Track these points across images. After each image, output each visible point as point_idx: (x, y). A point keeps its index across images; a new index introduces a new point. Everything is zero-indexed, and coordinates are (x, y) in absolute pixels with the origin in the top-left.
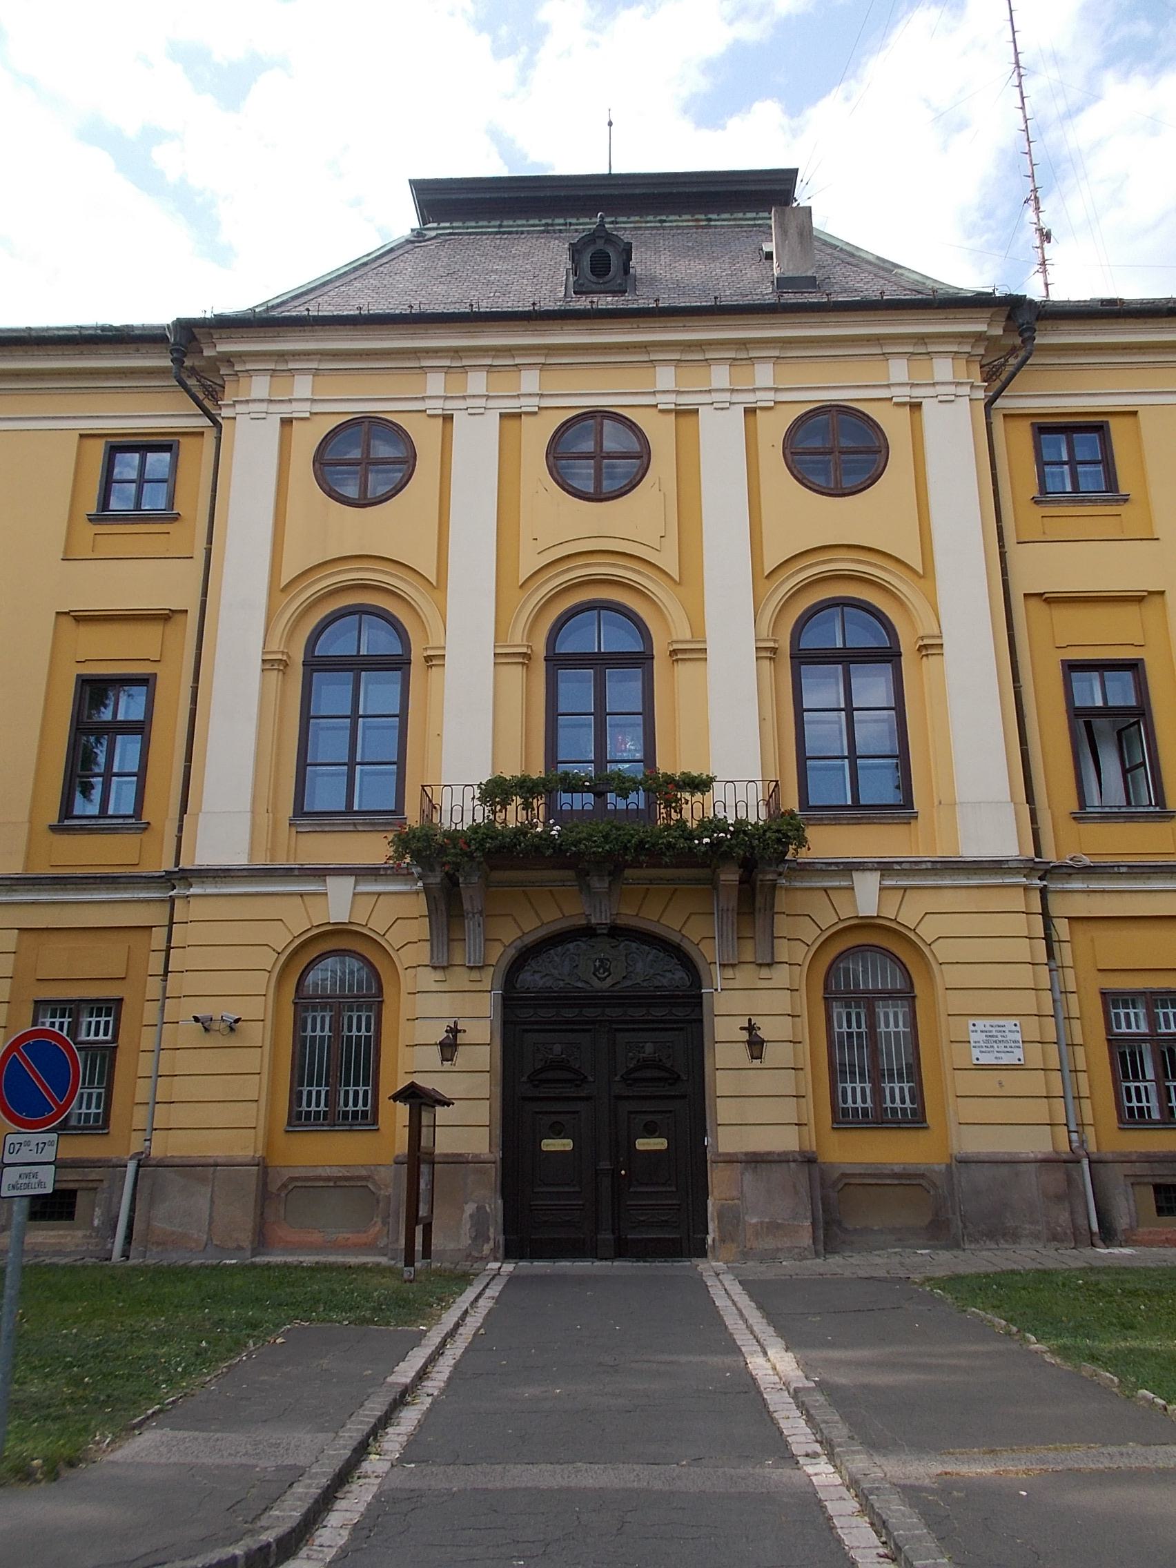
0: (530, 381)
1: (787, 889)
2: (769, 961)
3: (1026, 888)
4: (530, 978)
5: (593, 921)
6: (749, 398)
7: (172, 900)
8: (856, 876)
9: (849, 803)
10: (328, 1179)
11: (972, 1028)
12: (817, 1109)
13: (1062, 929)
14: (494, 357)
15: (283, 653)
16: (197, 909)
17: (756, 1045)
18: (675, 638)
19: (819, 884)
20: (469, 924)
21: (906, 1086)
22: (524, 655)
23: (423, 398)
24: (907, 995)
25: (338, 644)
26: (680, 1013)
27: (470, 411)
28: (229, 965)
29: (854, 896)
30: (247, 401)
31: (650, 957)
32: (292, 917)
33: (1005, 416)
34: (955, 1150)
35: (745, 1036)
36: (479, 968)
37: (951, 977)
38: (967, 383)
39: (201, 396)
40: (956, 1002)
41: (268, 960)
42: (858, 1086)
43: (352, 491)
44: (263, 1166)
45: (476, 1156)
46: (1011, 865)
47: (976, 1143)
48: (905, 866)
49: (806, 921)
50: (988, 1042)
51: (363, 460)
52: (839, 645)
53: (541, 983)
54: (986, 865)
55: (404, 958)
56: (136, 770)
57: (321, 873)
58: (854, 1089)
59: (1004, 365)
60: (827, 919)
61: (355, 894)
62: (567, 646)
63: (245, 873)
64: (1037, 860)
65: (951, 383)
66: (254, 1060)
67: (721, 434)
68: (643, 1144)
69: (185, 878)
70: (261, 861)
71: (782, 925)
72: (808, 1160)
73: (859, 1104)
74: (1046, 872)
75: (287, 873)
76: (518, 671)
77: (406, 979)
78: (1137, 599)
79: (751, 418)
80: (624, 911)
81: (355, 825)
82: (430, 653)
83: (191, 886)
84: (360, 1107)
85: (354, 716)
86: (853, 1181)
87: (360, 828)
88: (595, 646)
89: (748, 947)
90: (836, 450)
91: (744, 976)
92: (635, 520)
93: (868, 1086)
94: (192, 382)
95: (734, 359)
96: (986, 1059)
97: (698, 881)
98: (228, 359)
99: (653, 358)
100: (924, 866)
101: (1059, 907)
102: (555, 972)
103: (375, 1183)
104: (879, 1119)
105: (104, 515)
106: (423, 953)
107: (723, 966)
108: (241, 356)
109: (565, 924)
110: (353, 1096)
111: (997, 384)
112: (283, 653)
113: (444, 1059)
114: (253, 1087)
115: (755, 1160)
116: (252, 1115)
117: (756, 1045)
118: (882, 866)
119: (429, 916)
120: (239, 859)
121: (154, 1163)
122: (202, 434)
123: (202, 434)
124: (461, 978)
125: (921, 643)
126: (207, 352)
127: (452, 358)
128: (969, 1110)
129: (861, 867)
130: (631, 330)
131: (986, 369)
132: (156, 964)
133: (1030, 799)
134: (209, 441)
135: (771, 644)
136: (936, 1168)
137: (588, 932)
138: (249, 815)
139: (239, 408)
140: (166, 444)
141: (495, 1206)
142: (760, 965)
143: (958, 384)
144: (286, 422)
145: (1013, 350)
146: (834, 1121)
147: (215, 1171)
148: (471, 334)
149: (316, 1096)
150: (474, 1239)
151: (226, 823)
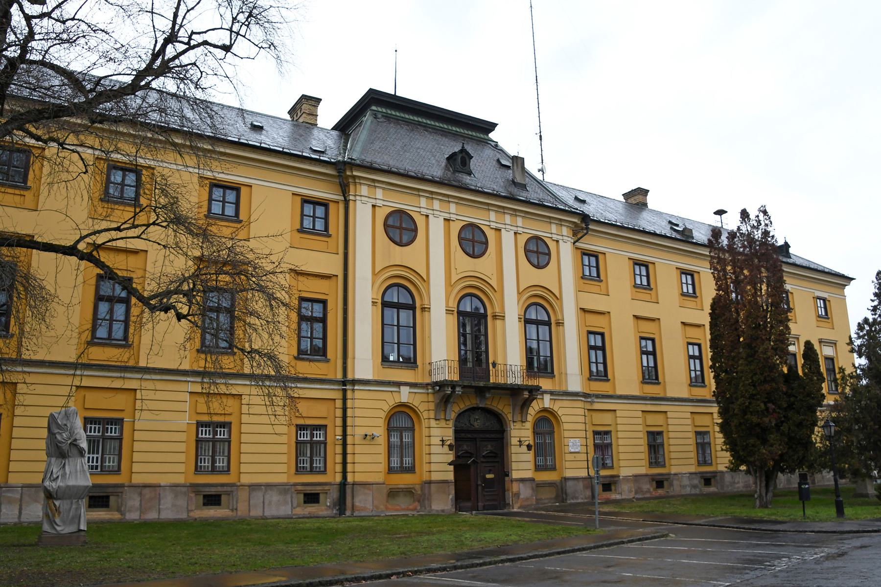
6: (374, 201)
8: (402, 387)
24: (412, 429)
26: (463, 435)
28: (369, 414)
32: (389, 399)
37: (566, 426)
47: (569, 474)
49: (535, 407)
51: (400, 228)
55: (425, 415)
57: (398, 384)
77: (425, 423)
78: (652, 320)
91: (518, 425)
92: (484, 266)
96: (572, 450)
98: (354, 177)
105: (302, 230)
106: (432, 415)
108: (360, 177)
115: (522, 480)
120: (370, 377)
124: (443, 423)
130: (518, 205)
132: (339, 413)
139: (358, 198)
140: (325, 204)
145: (582, 229)
148: (439, 188)
149: (319, 437)
151: (365, 363)
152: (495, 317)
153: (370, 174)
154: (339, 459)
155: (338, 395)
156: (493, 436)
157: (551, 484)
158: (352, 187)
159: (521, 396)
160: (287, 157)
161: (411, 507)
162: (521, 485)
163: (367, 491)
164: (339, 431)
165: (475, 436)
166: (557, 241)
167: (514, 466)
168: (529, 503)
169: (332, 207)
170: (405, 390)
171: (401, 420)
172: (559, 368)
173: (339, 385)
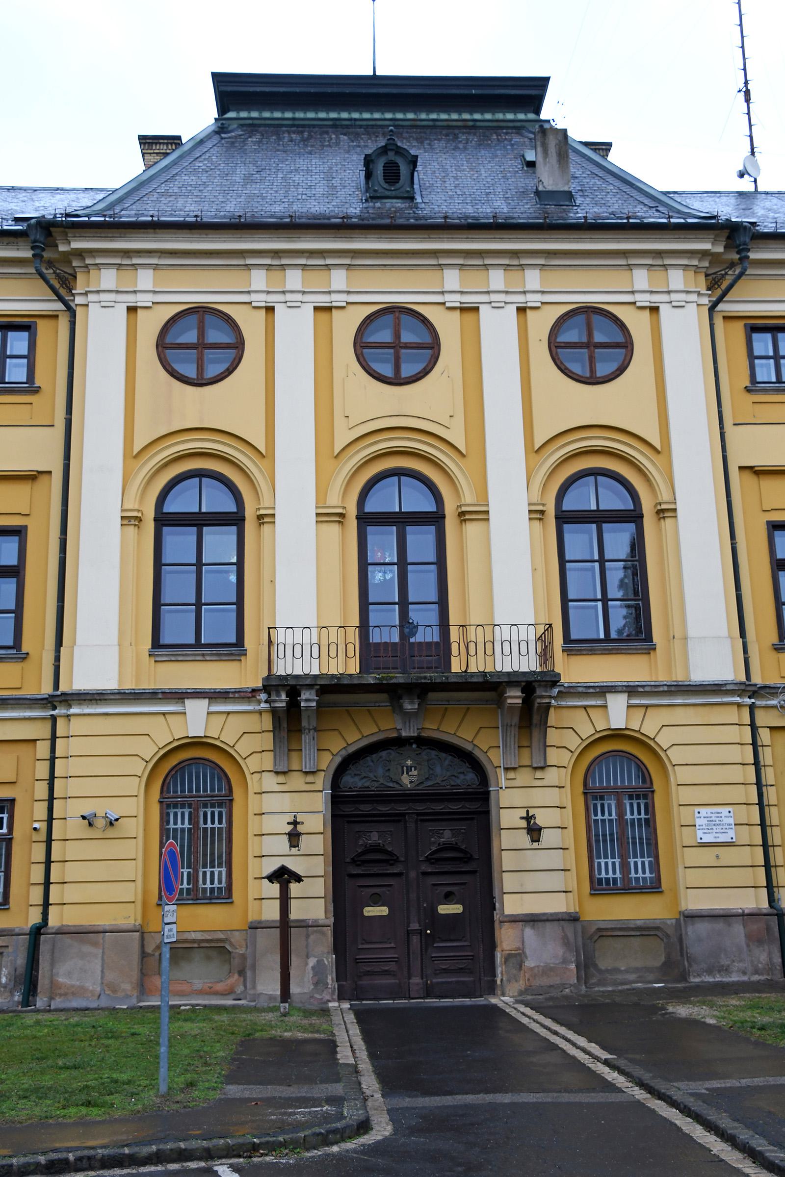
0: (339, 279)
1: (556, 707)
2: (542, 765)
3: (739, 705)
4: (352, 781)
5: (404, 734)
6: (520, 299)
7: (54, 719)
8: (609, 696)
9: (602, 636)
10: (194, 941)
11: (697, 815)
12: (576, 879)
13: (765, 736)
14: (308, 258)
15: (138, 511)
16: (77, 726)
17: (534, 831)
18: (463, 502)
19: (580, 704)
20: (306, 738)
21: (646, 861)
22: (341, 514)
23: (249, 292)
25: (182, 502)
27: (494, 305)
28: (107, 773)
29: (607, 713)
30: (98, 292)
31: (447, 762)
32: (161, 730)
33: (725, 318)
34: (683, 907)
35: (524, 824)
36: (313, 773)
37: (682, 775)
38: (695, 292)
39: (57, 286)
40: (685, 795)
41: (139, 768)
42: (610, 861)
43: (190, 371)
44: (142, 932)
45: (316, 920)
46: (729, 687)
47: (695, 902)
48: (647, 689)
49: (571, 731)
50: (709, 825)
51: (200, 346)
52: (397, 510)
53: (360, 784)
54: (709, 688)
55: (251, 765)
56: (13, 607)
57: (180, 696)
58: (606, 864)
59: (723, 276)
60: (587, 731)
61: (208, 713)
62: (172, 506)
63: (117, 697)
64: (748, 683)
65: (648, 291)
66: (133, 849)
67: (498, 328)
68: (444, 909)
69: (66, 701)
70: (129, 685)
71: (552, 737)
72: (573, 919)
73: (611, 875)
74: (754, 692)
75: (153, 696)
76: (335, 528)
77: (253, 783)
79: (132, 316)
80: (427, 726)
81: (203, 655)
82: (262, 512)
83: (70, 706)
84: (216, 885)
85: (199, 564)
86: (604, 934)
87: (208, 658)
88: (402, 511)
89: (526, 752)
90: (591, 346)
91: (523, 777)
92: (429, 401)
93: (617, 861)
94: (48, 272)
95: (508, 265)
96: (707, 839)
97: (487, 702)
98: (80, 254)
99: (522, 262)
100: (661, 689)
101: (764, 719)
102: (371, 775)
103: (231, 944)
104: (627, 888)
106: (268, 761)
107: (507, 769)
108: (93, 252)
109: (381, 736)
110: (212, 877)
111: (719, 292)
112: (138, 511)
113: (533, 841)
114: (132, 870)
115: (533, 920)
116: (130, 892)
117: (534, 831)
118: (629, 689)
119: (273, 731)
120: (111, 684)
121: (54, 931)
122: (57, 316)
123: (57, 316)
124: (297, 781)
125: (659, 507)
126: (62, 248)
127: (273, 258)
128: (693, 877)
129: (612, 689)
131: (710, 278)
132: (42, 770)
133: (743, 634)
134: (63, 324)
135: (540, 508)
136: (669, 922)
137: (398, 743)
138: (117, 648)
139: (92, 297)
141: (330, 960)
142: (536, 768)
143: (688, 292)
144: (132, 310)
145: (732, 265)
146: (592, 888)
147: (104, 937)
148: (290, 239)
149: (609, 868)
150: (316, 984)
152: (463, 516)
153: (112, 238)
154: (37, 874)
155: (41, 731)
156: (454, 807)
157: (647, 931)
158: (80, 277)
159: (526, 702)
160: (682, 233)
161: (220, 987)
162: (529, 932)
163: (87, 948)
164: (41, 811)
165: (401, 808)
166: (654, 310)
167: (509, 882)
168: (556, 980)
169: (42, 326)
170: (197, 709)
171: (193, 783)
172: (667, 626)
173: (44, 707)
